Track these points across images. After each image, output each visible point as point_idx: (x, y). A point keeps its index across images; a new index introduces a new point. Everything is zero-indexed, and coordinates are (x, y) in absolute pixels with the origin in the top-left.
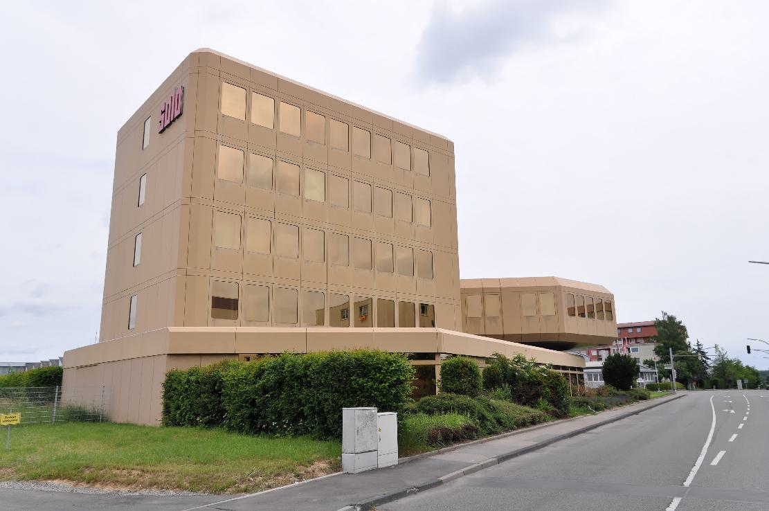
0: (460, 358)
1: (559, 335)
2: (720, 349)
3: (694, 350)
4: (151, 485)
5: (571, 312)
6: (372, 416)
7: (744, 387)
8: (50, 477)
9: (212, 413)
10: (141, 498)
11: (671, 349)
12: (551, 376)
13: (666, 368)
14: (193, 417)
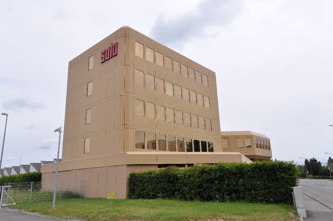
1: (253, 156)
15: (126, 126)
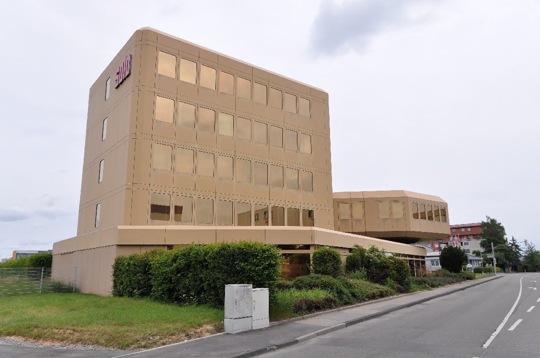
3: (510, 243)
4: (78, 341)
5: (416, 216)
6: (249, 290)
8: (9, 334)
9: (144, 287)
11: (492, 243)
14: (131, 290)
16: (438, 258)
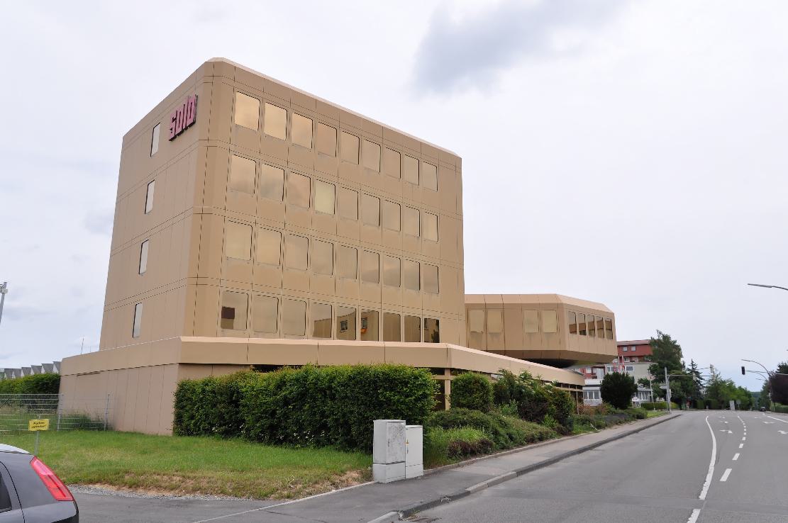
0: (472, 373)
1: (560, 352)
2: (714, 370)
3: (689, 370)
4: (194, 490)
5: (573, 331)
6: (401, 428)
7: (737, 408)
8: (91, 482)
9: (228, 423)
10: (188, 502)
12: (557, 393)
13: (661, 387)
14: (207, 426)
15: (200, 281)
16: (598, 388)
